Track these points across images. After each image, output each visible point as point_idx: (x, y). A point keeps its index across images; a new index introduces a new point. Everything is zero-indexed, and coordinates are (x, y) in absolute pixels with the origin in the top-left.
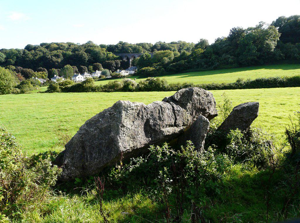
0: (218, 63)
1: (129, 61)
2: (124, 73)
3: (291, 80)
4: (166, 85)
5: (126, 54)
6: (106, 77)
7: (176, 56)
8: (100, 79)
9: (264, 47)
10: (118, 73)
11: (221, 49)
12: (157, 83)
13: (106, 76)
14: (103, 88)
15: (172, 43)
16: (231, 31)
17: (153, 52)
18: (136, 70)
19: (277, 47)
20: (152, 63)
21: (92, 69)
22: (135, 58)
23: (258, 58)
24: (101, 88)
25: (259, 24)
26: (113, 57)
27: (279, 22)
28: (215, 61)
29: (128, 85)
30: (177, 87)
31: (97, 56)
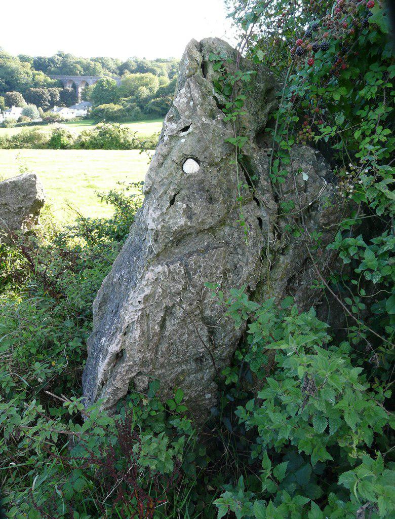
2: (66, 113)
5: (72, 77)
6: (32, 121)
7: (162, 86)
8: (19, 123)
10: (54, 113)
13: (32, 117)
15: (157, 61)
17: (123, 76)
18: (90, 109)
20: (118, 97)
21: (4, 103)
22: (87, 84)
24: (7, 140)
26: (45, 81)
29: (60, 136)
31: (12, 77)
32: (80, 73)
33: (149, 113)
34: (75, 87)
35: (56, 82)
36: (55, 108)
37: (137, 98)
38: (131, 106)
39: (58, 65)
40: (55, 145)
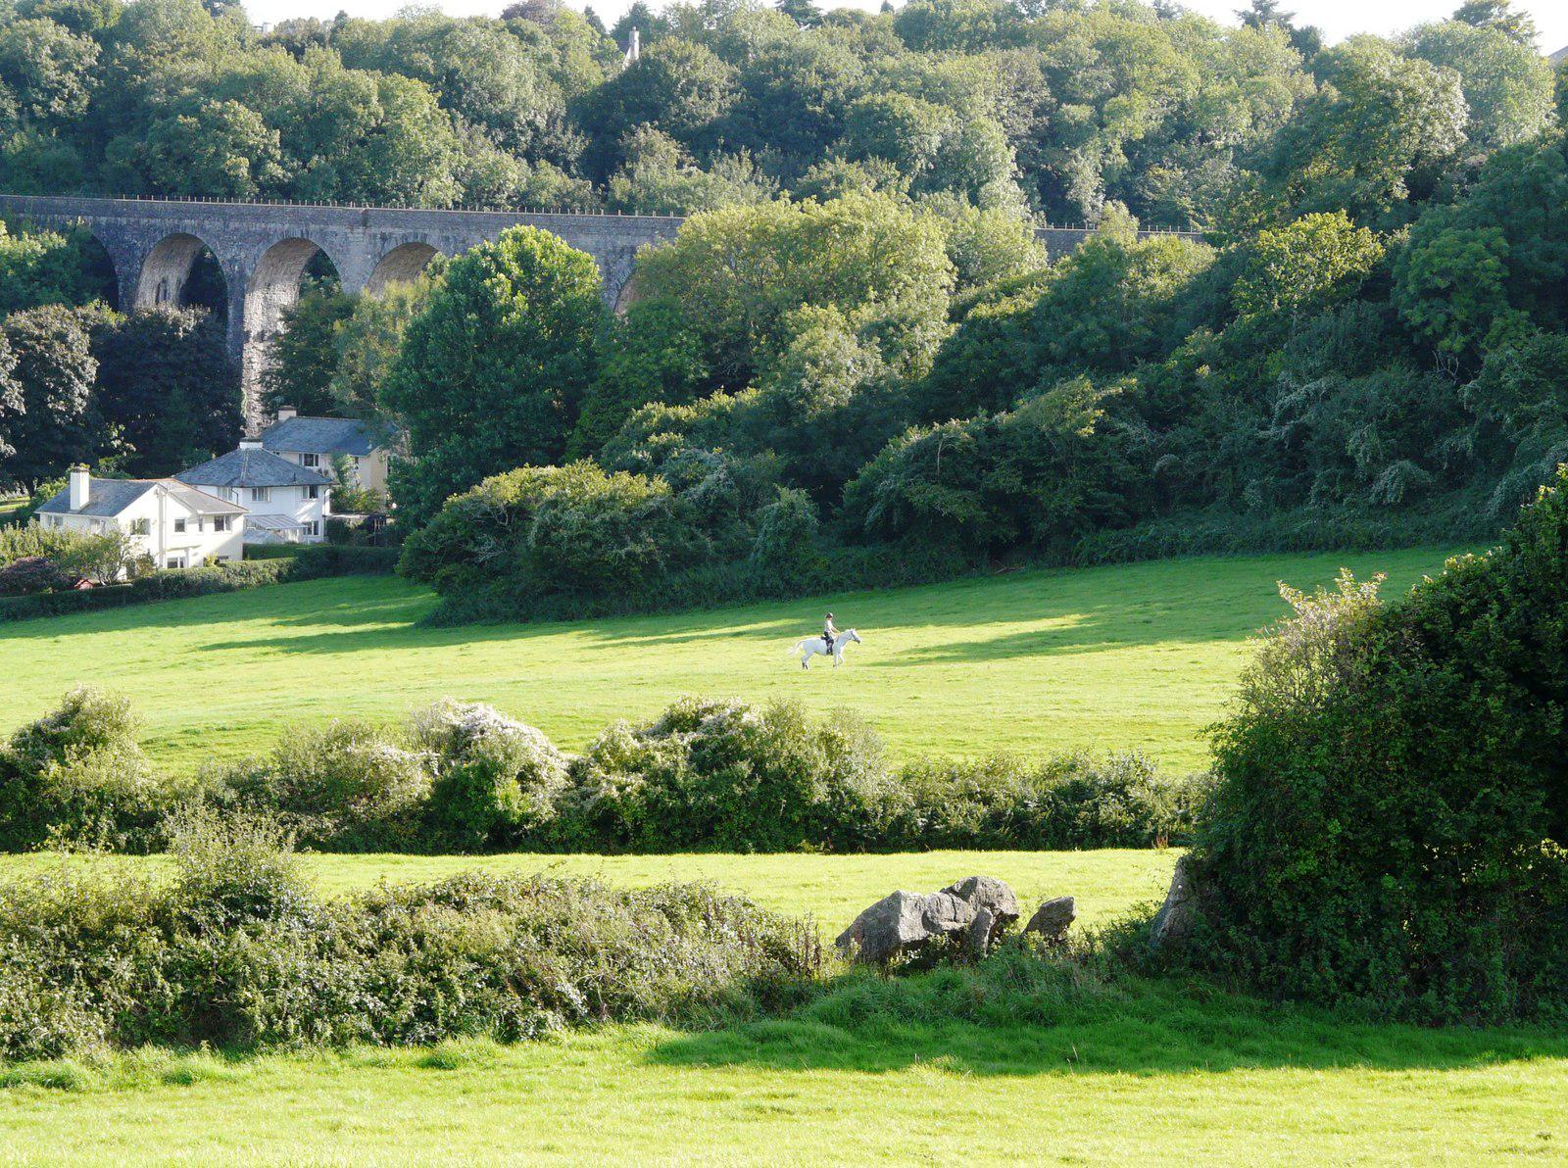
1: (222, 314)
2: (170, 524)
10: (77, 530)
12: (776, 755)
14: (231, 806)
18: (368, 474)
20: (621, 396)
29: (488, 772)
30: (987, 801)
32: (256, 168)
33: (886, 532)
34: (211, 288)
35: (53, 254)
36: (81, 484)
37: (783, 409)
38: (738, 479)
39: (57, 106)
40: (460, 825)
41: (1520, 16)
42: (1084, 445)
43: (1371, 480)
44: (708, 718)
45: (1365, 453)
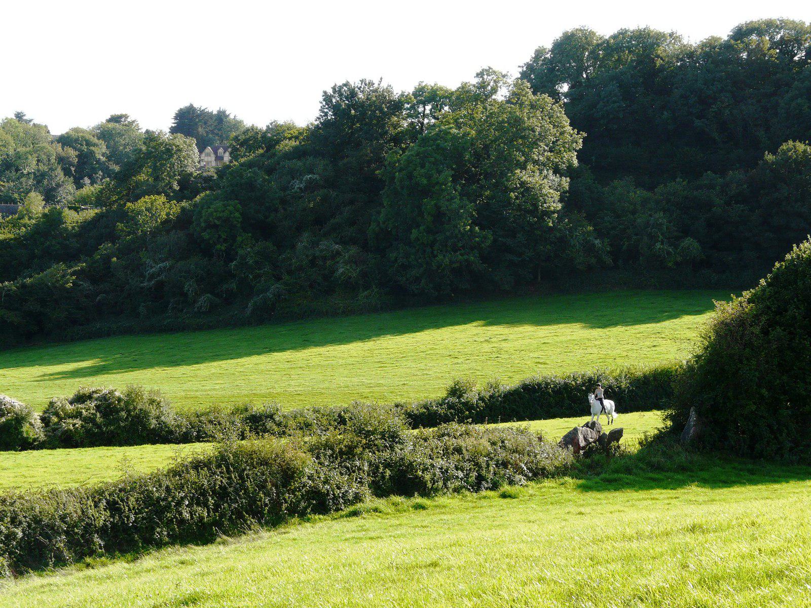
0: (275, 287)
3: (644, 383)
4: (170, 419)
9: (508, 202)
11: (283, 201)
12: (135, 408)
16: (327, 98)
19: (570, 199)
23: (484, 258)
25: (475, 81)
27: (562, 62)
28: (259, 276)
41: (133, 122)
42: (68, 291)
43: (195, 302)
44: (95, 395)
45: (192, 291)
